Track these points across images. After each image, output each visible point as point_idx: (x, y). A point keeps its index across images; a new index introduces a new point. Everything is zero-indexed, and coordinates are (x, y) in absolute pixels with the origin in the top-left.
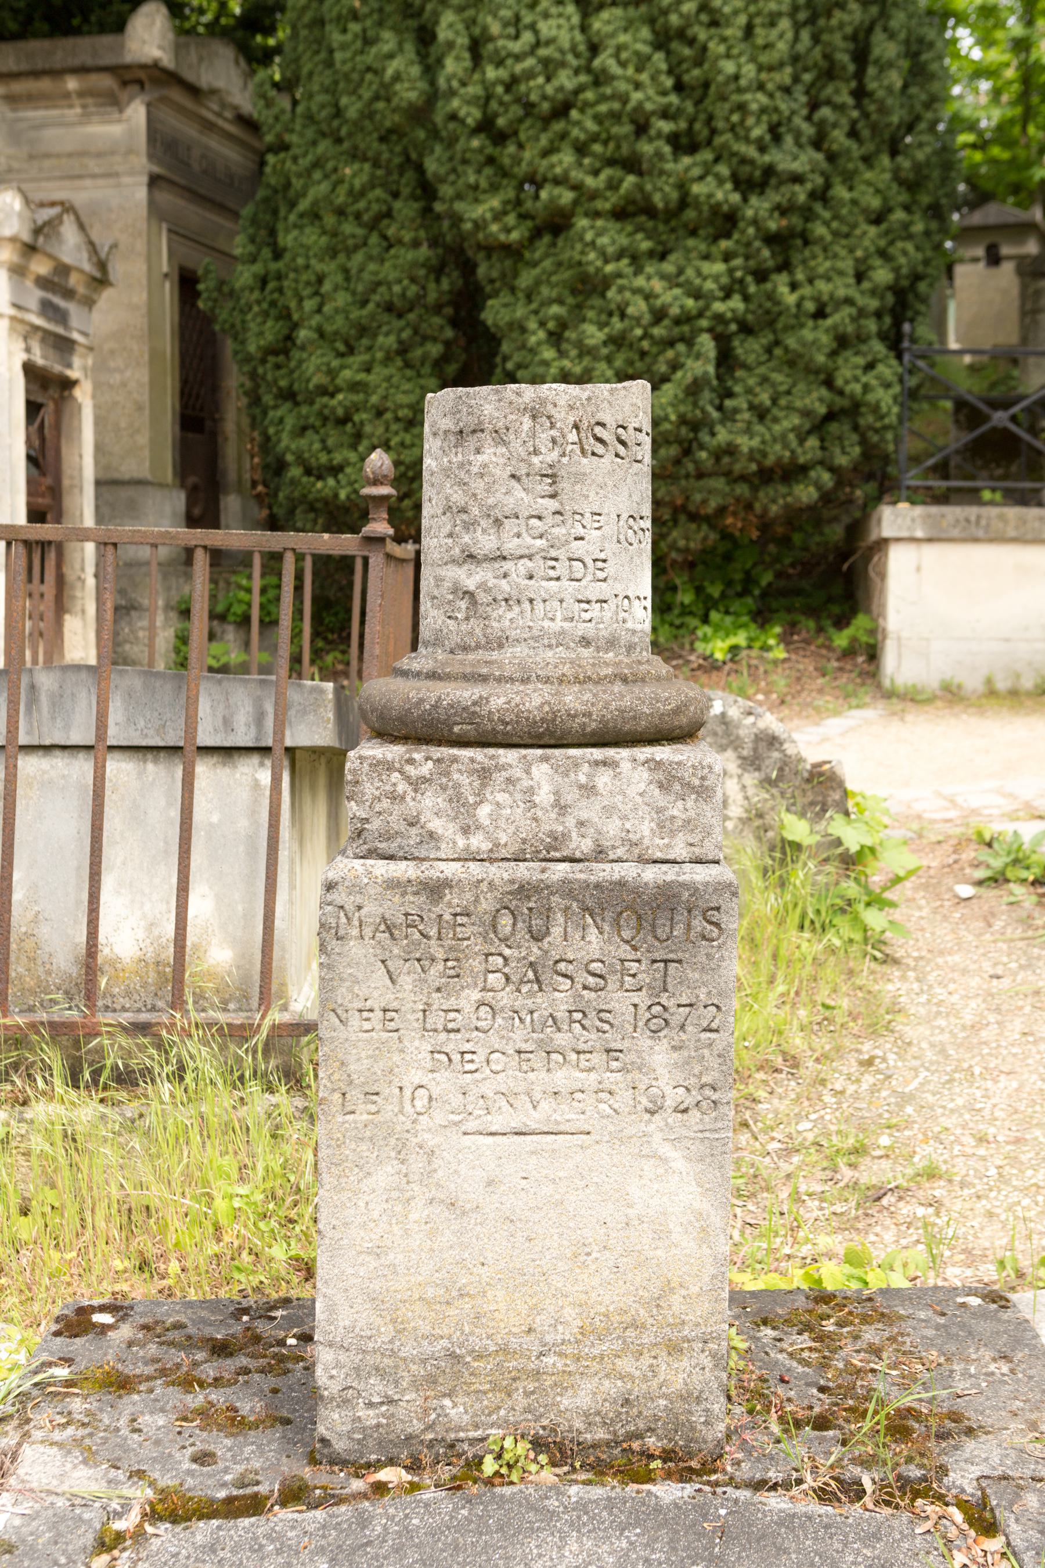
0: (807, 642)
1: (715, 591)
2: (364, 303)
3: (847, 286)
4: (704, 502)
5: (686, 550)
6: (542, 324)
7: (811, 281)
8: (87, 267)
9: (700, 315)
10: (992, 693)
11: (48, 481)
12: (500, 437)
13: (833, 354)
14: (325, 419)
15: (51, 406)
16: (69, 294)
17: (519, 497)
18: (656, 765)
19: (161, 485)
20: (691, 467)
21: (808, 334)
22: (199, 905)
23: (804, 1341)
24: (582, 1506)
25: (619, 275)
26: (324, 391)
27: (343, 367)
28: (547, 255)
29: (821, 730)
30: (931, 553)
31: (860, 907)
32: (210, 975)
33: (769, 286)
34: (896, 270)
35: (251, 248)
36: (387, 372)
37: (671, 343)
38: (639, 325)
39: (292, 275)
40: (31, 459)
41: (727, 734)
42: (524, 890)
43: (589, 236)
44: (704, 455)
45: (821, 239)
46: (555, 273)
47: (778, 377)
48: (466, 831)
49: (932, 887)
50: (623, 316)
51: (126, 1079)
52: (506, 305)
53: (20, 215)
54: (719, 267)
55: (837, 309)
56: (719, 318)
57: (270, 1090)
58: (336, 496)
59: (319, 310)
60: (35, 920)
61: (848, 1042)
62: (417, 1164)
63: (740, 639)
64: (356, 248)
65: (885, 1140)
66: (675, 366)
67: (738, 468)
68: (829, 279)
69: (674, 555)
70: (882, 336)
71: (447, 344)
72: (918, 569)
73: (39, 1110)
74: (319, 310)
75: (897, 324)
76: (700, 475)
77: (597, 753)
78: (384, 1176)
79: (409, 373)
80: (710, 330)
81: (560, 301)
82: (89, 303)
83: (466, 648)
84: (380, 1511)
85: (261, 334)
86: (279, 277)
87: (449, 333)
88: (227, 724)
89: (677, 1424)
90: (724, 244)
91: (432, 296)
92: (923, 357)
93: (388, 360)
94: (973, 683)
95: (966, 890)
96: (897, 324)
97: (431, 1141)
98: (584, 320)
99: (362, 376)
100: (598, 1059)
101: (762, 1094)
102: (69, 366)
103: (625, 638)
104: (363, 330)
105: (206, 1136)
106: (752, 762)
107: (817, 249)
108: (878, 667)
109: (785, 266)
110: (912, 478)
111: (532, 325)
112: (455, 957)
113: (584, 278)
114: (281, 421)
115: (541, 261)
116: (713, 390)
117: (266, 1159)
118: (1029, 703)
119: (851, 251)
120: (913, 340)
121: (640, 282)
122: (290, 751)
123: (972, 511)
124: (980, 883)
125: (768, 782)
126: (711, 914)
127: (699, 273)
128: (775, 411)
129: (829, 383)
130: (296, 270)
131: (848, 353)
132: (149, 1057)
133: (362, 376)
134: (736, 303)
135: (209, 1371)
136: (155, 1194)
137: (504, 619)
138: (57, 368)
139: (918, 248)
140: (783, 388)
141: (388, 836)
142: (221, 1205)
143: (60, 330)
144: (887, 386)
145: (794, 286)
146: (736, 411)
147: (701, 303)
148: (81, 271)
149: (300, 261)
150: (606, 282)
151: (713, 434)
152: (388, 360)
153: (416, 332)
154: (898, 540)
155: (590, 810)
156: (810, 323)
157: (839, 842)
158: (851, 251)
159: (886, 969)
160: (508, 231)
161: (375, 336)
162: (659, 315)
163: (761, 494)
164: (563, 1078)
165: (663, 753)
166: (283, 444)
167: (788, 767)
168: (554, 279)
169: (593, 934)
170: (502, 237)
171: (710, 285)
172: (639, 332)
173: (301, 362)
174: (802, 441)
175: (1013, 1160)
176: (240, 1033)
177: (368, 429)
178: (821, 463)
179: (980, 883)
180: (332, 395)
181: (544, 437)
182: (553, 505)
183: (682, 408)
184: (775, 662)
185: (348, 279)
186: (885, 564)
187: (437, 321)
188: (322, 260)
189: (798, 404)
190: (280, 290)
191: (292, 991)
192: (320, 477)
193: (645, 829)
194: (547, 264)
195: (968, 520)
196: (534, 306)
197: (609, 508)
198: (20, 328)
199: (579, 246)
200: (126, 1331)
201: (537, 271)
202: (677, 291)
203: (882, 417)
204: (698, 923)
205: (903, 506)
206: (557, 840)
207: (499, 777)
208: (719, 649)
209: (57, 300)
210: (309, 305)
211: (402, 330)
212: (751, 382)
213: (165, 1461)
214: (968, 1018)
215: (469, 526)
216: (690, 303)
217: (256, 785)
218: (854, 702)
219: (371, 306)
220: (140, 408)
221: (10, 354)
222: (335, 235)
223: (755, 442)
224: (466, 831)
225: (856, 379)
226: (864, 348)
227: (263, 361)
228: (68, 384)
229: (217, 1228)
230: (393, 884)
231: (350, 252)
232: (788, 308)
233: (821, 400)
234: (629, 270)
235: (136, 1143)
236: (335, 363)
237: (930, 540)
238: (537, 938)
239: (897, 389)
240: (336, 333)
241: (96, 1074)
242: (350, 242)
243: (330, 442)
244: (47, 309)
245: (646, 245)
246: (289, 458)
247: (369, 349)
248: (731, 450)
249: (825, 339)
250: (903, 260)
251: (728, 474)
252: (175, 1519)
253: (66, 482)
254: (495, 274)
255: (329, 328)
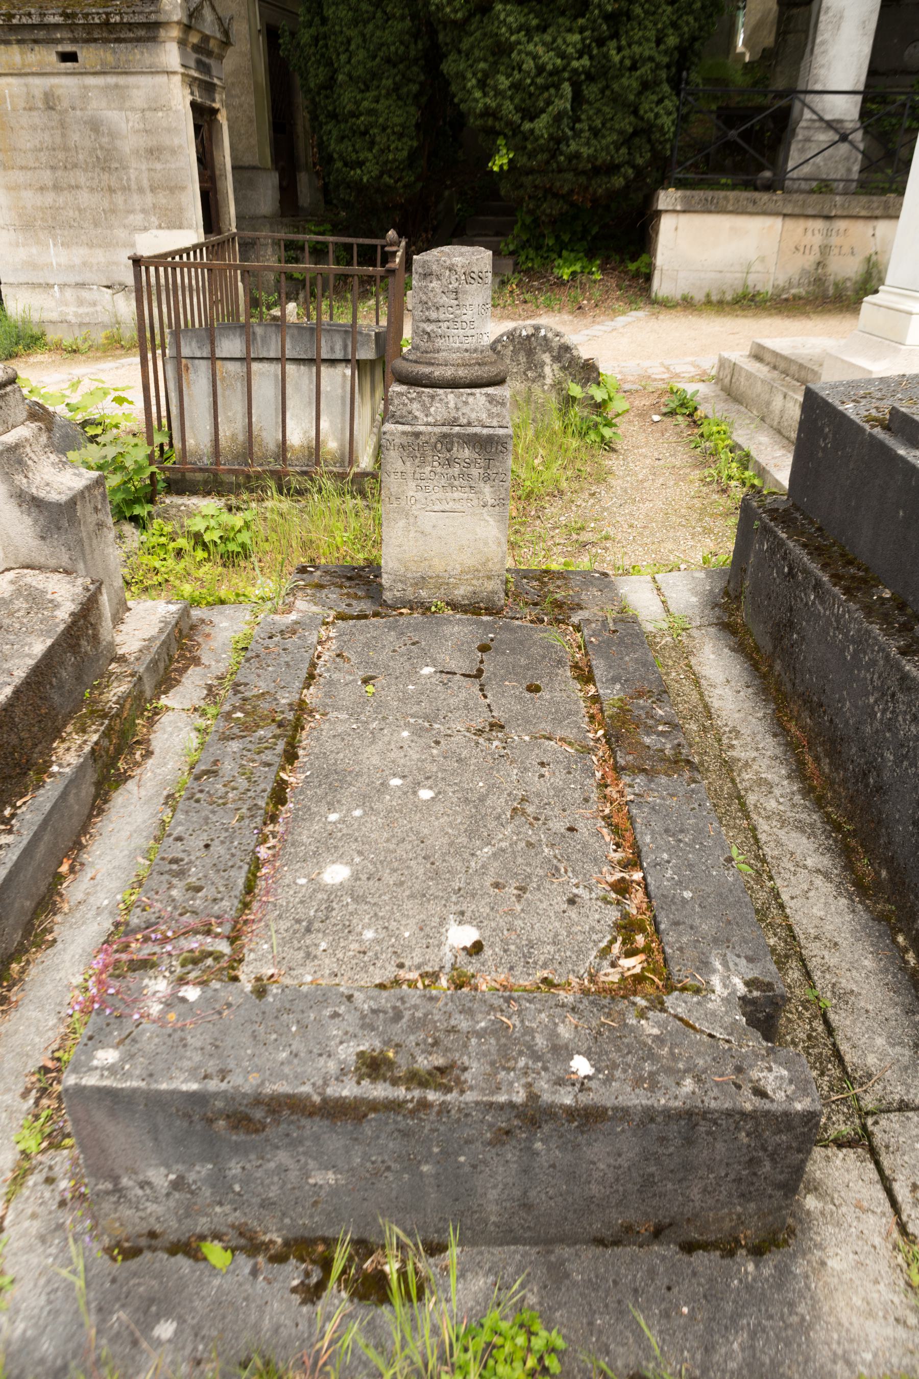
0: (614, 269)
1: (566, 238)
2: (374, 57)
3: (651, 49)
4: (562, 187)
5: (550, 215)
6: (474, 74)
7: (629, 46)
8: (218, 35)
9: (564, 69)
10: (708, 302)
11: (208, 173)
12: (438, 278)
13: (640, 94)
14: (354, 132)
15: (206, 126)
16: (209, 54)
17: (444, 300)
18: (487, 395)
19: (265, 169)
20: (555, 165)
21: (625, 81)
22: (324, 424)
23: (536, 583)
24: (460, 619)
25: (519, 42)
26: (353, 115)
27: (363, 99)
28: (478, 29)
29: (613, 323)
30: (684, 219)
31: (601, 427)
32: (329, 453)
33: (605, 49)
34: (681, 36)
35: (308, 17)
36: (387, 103)
37: (546, 88)
38: (529, 76)
39: (333, 37)
40: (200, 160)
41: (547, 345)
42: (445, 436)
43: (502, 17)
44: (562, 158)
45: (638, 16)
46: (482, 40)
47: (606, 109)
48: (427, 416)
49: (643, 414)
50: (520, 70)
51: (300, 492)
52: (454, 61)
53: (181, 6)
54: (576, 37)
55: (643, 65)
56: (575, 71)
57: (354, 497)
58: (361, 179)
59: (349, 62)
60: (260, 430)
61: (586, 486)
62: (412, 520)
63: (577, 268)
64: (369, 20)
65: (592, 525)
66: (549, 103)
67: (581, 166)
68: (640, 44)
69: (543, 218)
70: (669, 80)
71: (422, 84)
72: (676, 229)
73: (269, 504)
74: (349, 62)
75: (679, 72)
76: (560, 171)
77: (469, 391)
78: (402, 523)
79: (400, 103)
80: (569, 79)
81: (485, 60)
82: (220, 58)
83: (427, 352)
84: (402, 620)
85: (317, 75)
86: (325, 37)
87: (422, 78)
88: (332, 349)
89: (489, 600)
90: (581, 21)
91: (413, 53)
92: (692, 94)
93: (388, 95)
94: (699, 296)
95: (656, 418)
96: (679, 72)
97: (416, 513)
98: (498, 72)
99: (374, 105)
100: (467, 489)
101: (547, 505)
102: (214, 101)
103: (480, 348)
104: (374, 75)
105: (331, 514)
106: (557, 359)
107: (635, 23)
108: (650, 286)
109: (615, 35)
110: (678, 174)
111: (469, 75)
112: (423, 456)
113: (498, 44)
114: (330, 132)
115: (475, 32)
116: (569, 117)
117: (353, 523)
118: (727, 309)
119: (655, 24)
120: (687, 83)
121: (531, 47)
122: (358, 361)
123: (709, 194)
124: (665, 414)
125: (563, 368)
126: (504, 444)
127: (565, 42)
128: (604, 131)
129: (635, 112)
130: (334, 34)
131: (648, 93)
132: (309, 485)
133: (374, 105)
134: (585, 61)
135: (347, 584)
136: (313, 536)
137: (440, 343)
138: (208, 103)
139: (696, 19)
140: (610, 116)
141: (402, 417)
142: (338, 539)
143: (207, 78)
144: (669, 114)
145: (619, 49)
146: (582, 131)
147: (565, 61)
148: (215, 38)
149: (337, 28)
150: (511, 47)
151: (568, 146)
152: (388, 95)
153: (403, 76)
154: (667, 211)
155: (465, 410)
156: (627, 74)
157: (592, 398)
158: (655, 24)
159: (611, 454)
160: (456, 11)
161: (381, 79)
162: (540, 69)
163: (593, 182)
164: (456, 495)
165: (490, 390)
166: (332, 147)
167: (574, 360)
168: (482, 44)
169: (466, 450)
170: (452, 16)
171: (571, 50)
172: (529, 81)
173: (339, 95)
174: (617, 149)
175: (641, 534)
176: (341, 476)
177: (378, 139)
178: (628, 163)
179: (665, 414)
180: (358, 117)
181: (453, 277)
182: (456, 302)
183: (551, 130)
184: (595, 282)
185: (364, 41)
186: (658, 225)
187: (415, 69)
188: (349, 28)
189: (617, 126)
190: (326, 46)
191: (360, 460)
192: (352, 168)
193: (484, 416)
194: (478, 34)
195: (706, 200)
196: (470, 62)
197: (476, 303)
198: (187, 79)
199: (496, 23)
200: (318, 573)
201: (472, 39)
202: (552, 54)
203: (664, 135)
204: (500, 448)
205: (671, 190)
206: (456, 419)
207: (437, 398)
208: (566, 273)
209: (207, 60)
210: (343, 58)
211: (396, 75)
212: (591, 112)
213: (338, 605)
214: (640, 477)
215: (428, 309)
216: (559, 61)
217: (344, 375)
218: (634, 306)
219: (378, 59)
220: (251, 121)
221: (184, 97)
222: (356, 10)
223: (591, 151)
224: (427, 416)
225: (651, 110)
226: (657, 89)
227: (319, 94)
228: (215, 112)
229: (338, 548)
230: (404, 433)
231: (366, 22)
232: (615, 65)
233: (630, 124)
234: (524, 39)
235: (305, 516)
236: (359, 97)
237: (684, 212)
238: (449, 451)
239: (675, 116)
240: (359, 77)
241: (288, 490)
242: (366, 16)
243: (357, 146)
244: (201, 66)
245: (534, 22)
246: (335, 156)
247: (378, 87)
248: (577, 155)
249: (635, 85)
250: (686, 29)
251: (575, 170)
252: (343, 619)
253: (217, 172)
254: (448, 40)
255: (355, 74)
